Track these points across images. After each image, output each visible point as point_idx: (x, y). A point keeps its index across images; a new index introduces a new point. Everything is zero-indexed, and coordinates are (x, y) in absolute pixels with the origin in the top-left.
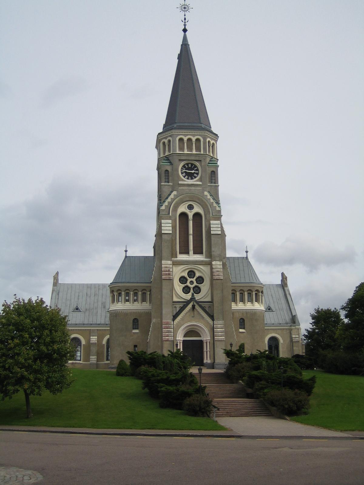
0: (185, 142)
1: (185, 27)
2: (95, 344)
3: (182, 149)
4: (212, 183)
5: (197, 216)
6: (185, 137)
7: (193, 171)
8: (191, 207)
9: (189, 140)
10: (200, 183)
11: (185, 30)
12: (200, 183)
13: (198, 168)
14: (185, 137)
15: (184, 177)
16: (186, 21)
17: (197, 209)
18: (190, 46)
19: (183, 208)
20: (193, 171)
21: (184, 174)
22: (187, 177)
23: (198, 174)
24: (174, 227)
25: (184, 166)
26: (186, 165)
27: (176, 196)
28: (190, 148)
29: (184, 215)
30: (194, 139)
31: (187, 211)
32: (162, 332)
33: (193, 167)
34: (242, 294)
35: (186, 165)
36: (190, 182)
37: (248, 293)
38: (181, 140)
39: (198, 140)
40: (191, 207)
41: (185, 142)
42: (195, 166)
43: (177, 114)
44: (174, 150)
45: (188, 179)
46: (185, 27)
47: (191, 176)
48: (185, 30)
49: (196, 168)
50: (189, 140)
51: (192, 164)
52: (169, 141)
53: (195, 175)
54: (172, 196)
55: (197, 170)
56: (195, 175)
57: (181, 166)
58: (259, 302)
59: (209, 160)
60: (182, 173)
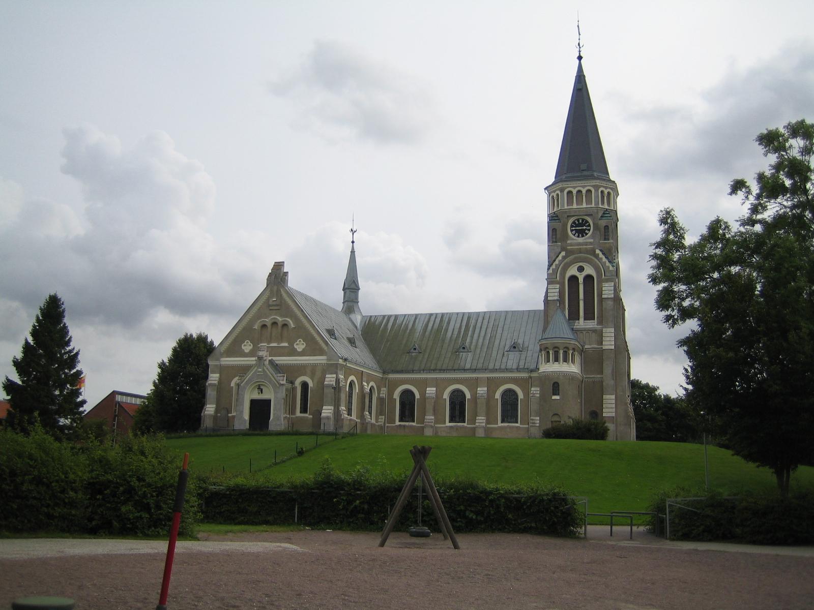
0: (584, 195)
1: (580, 54)
2: (214, 385)
3: (570, 202)
4: (605, 239)
5: (589, 278)
6: (584, 188)
7: (585, 228)
8: (581, 269)
9: (579, 192)
10: (592, 240)
11: (580, 58)
12: (592, 240)
13: (572, 223)
14: (584, 188)
15: (574, 235)
16: (581, 46)
17: (589, 270)
18: (576, 75)
19: (573, 271)
20: (585, 228)
21: (574, 232)
22: (577, 234)
23: (589, 230)
24: (561, 293)
25: (574, 222)
26: (576, 221)
27: (564, 258)
28: (579, 202)
29: (574, 279)
30: (584, 191)
31: (577, 274)
32: (616, 412)
33: (585, 223)
34: (565, 353)
35: (576, 221)
36: (581, 240)
37: (555, 351)
38: (570, 193)
39: (589, 191)
40: (581, 269)
41: (584, 195)
42: (587, 222)
43: (566, 164)
44: (564, 206)
45: (578, 237)
46: (580, 54)
47: (582, 233)
48: (580, 58)
49: (588, 224)
50: (579, 192)
51: (583, 220)
52: (558, 195)
53: (586, 231)
54: (560, 258)
55: (589, 226)
56: (586, 231)
57: (571, 222)
58: (574, 362)
59: (602, 212)
60: (572, 231)
